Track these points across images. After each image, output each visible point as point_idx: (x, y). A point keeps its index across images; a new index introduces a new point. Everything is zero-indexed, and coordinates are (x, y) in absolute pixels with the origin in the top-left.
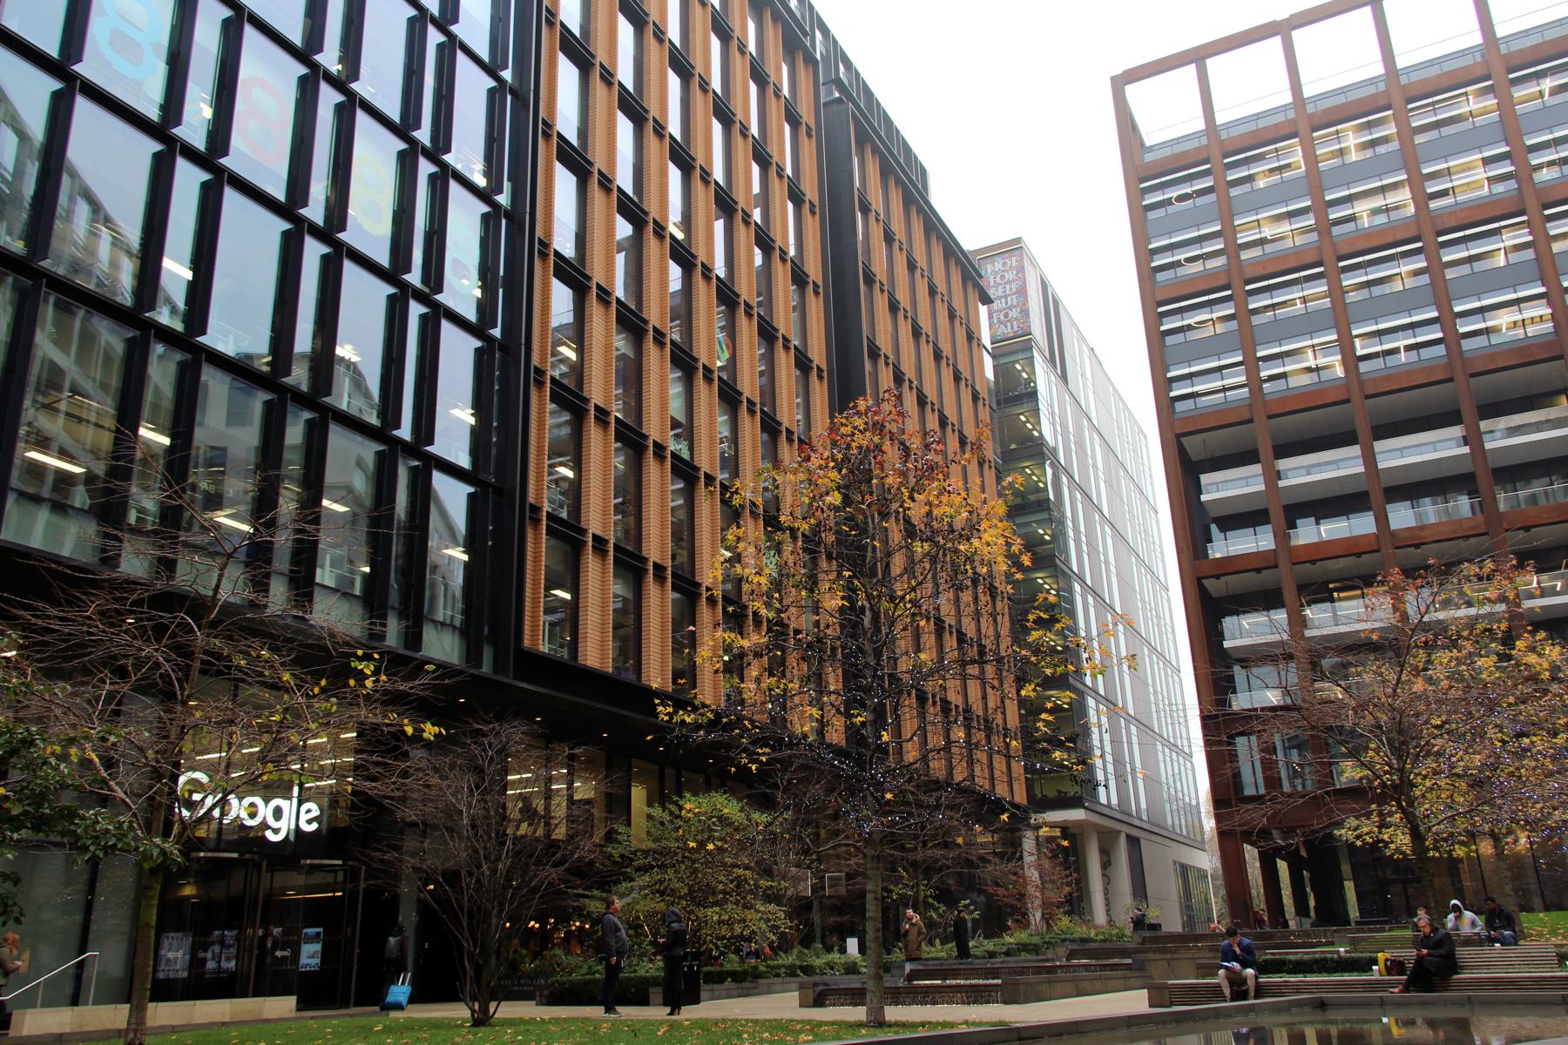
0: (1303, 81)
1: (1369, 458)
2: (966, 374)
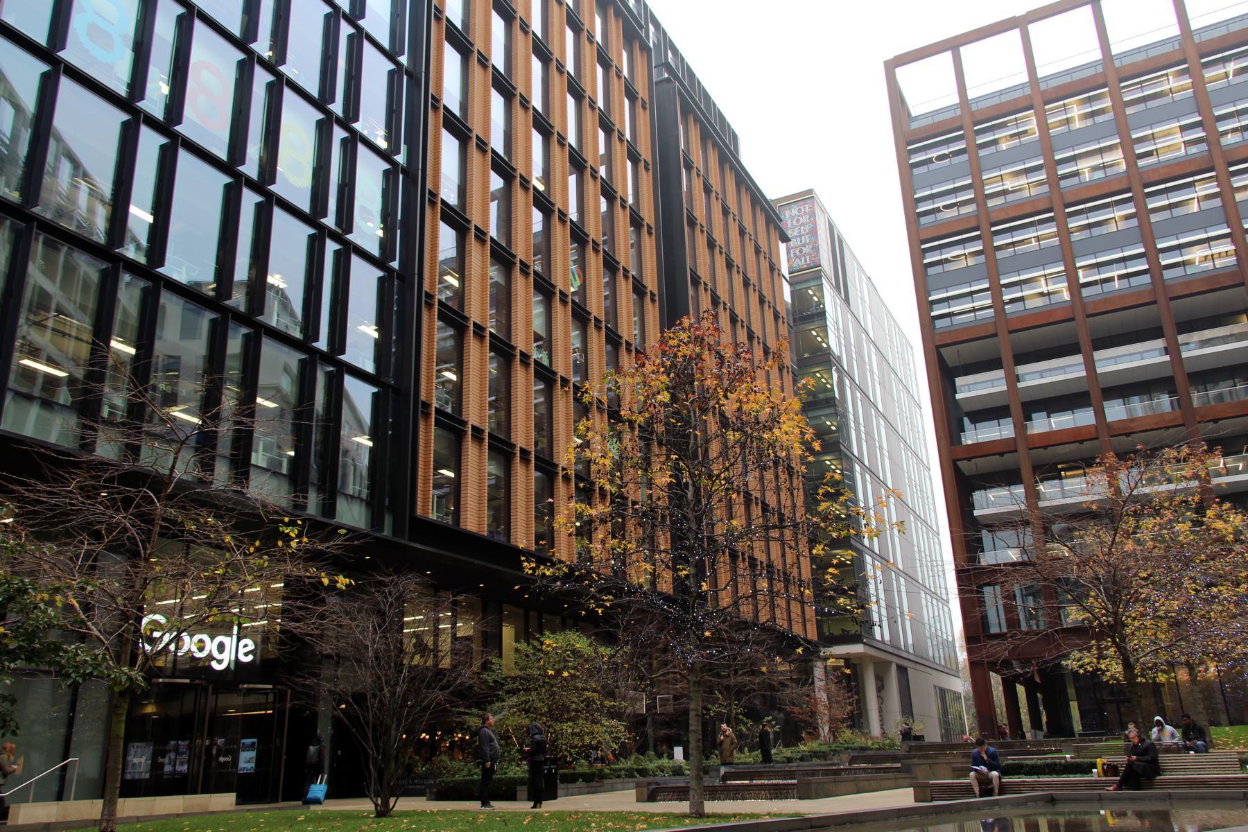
0: (1037, 65)
1: (1090, 365)
2: (769, 298)
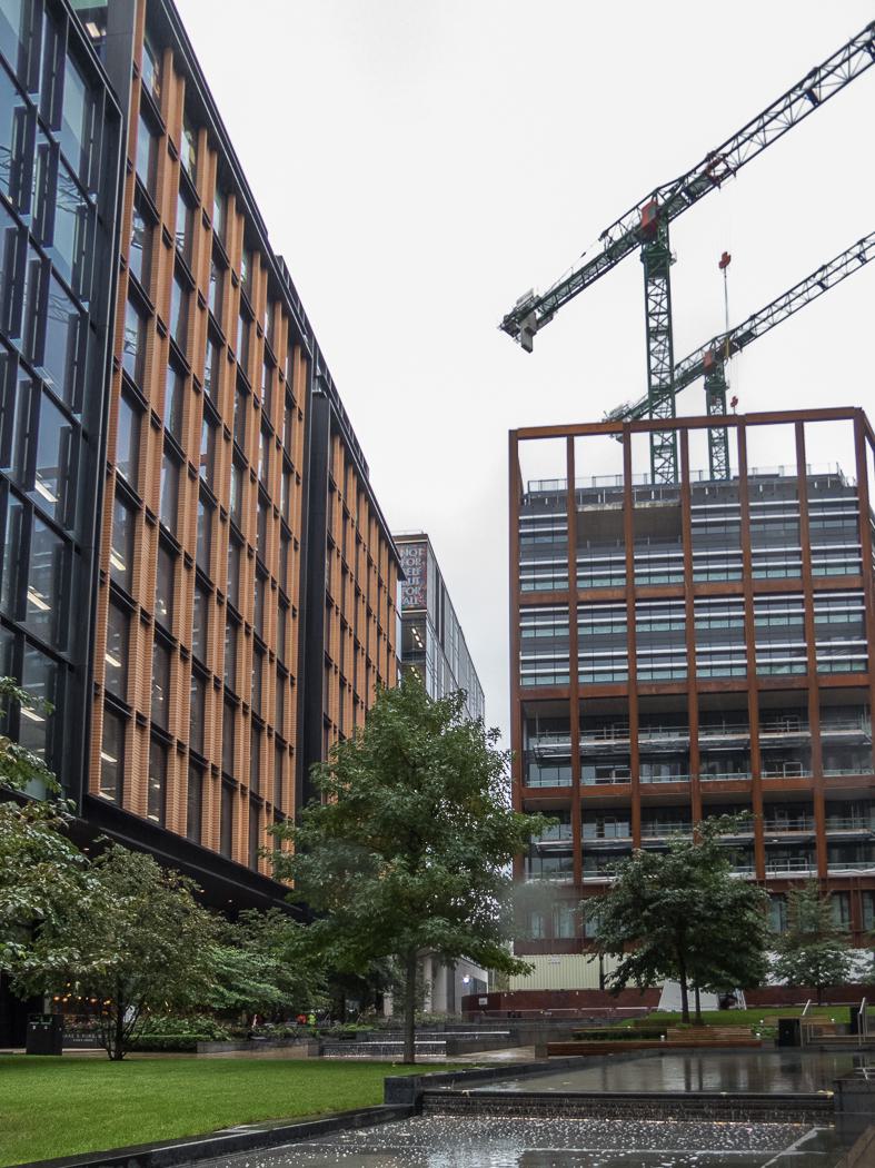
0: (576, 476)
2: (384, 631)
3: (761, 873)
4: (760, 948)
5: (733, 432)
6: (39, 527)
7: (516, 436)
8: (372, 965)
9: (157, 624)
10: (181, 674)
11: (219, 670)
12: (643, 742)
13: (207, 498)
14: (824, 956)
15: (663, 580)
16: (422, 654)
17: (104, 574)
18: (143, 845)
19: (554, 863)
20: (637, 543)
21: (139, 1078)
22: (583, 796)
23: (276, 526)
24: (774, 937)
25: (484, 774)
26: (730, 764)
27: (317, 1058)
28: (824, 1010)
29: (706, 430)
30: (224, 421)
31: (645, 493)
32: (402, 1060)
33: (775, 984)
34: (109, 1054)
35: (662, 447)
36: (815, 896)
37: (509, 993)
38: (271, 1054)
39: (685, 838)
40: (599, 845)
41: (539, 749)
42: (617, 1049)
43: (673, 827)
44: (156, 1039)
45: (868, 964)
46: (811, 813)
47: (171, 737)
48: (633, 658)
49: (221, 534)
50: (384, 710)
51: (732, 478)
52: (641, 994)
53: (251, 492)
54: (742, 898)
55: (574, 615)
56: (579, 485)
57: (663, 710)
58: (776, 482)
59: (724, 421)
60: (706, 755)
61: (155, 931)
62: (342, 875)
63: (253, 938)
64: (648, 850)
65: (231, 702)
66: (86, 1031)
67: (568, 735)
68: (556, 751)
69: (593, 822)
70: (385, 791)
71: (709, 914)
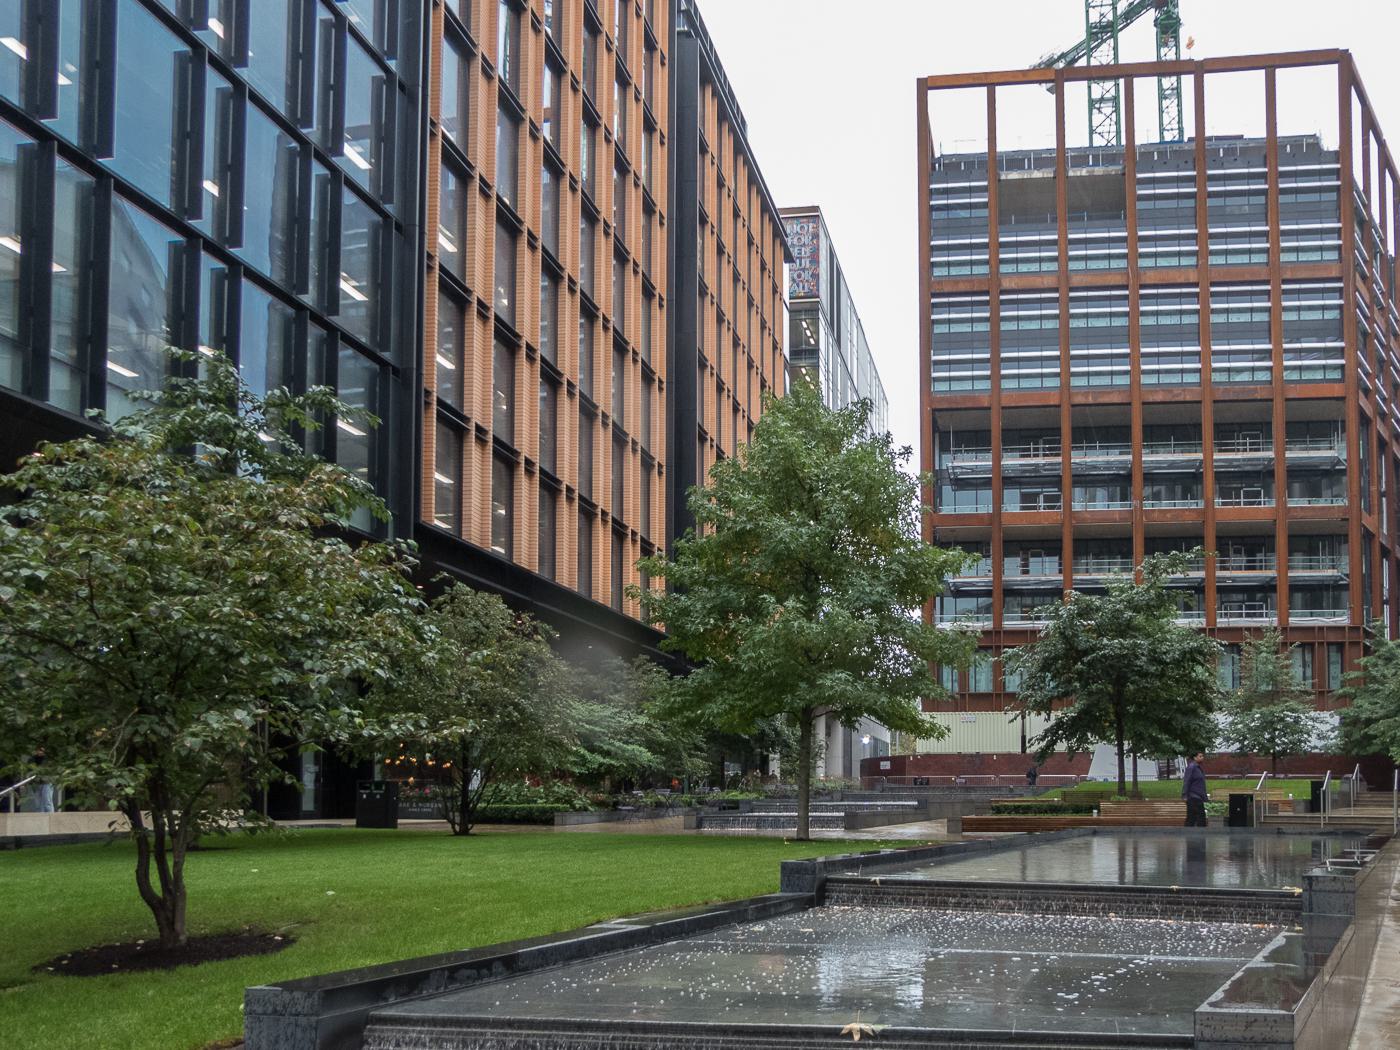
2: (769, 324)
3: (1211, 620)
4: (1210, 709)
5: (1188, 81)
6: (349, 198)
7: (925, 86)
8: (761, 724)
9: (497, 318)
10: (528, 377)
11: (572, 373)
12: (1077, 461)
13: (553, 163)
14: (1282, 720)
15: (1103, 264)
16: (814, 352)
17: (430, 257)
18: (493, 584)
19: (970, 603)
20: (1071, 219)
21: (493, 858)
22: (1006, 522)
23: (637, 196)
24: (1226, 696)
25: (893, 501)
26: (1179, 489)
27: (693, 832)
28: (1279, 783)
29: (1155, 79)
30: (571, 67)
31: (1081, 157)
32: (795, 835)
33: (1223, 750)
34: (453, 827)
35: (1102, 100)
36: (1273, 648)
37: (915, 756)
38: (639, 826)
39: (1125, 576)
40: (1023, 583)
41: (954, 468)
42: (1046, 827)
43: (1109, 564)
44: (506, 809)
45: (1332, 730)
46: (1272, 549)
47: (517, 453)
48: (996, 363)
49: (571, 205)
50: (774, 423)
51: (1186, 140)
52: (1070, 760)
53: (605, 155)
54: (1192, 651)
55: (995, 306)
56: (1001, 147)
57: (1102, 425)
58: (1239, 144)
59: (1177, 68)
60: (1150, 478)
61: (505, 685)
62: (725, 619)
63: (617, 691)
64: (1085, 591)
65: (588, 411)
66: (425, 799)
67: (988, 451)
68: (973, 470)
69: (1016, 555)
70: (778, 520)
71: (1153, 669)
